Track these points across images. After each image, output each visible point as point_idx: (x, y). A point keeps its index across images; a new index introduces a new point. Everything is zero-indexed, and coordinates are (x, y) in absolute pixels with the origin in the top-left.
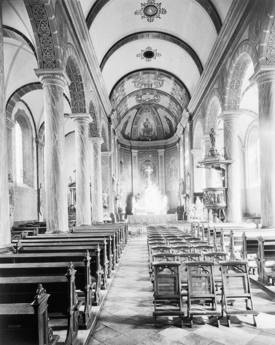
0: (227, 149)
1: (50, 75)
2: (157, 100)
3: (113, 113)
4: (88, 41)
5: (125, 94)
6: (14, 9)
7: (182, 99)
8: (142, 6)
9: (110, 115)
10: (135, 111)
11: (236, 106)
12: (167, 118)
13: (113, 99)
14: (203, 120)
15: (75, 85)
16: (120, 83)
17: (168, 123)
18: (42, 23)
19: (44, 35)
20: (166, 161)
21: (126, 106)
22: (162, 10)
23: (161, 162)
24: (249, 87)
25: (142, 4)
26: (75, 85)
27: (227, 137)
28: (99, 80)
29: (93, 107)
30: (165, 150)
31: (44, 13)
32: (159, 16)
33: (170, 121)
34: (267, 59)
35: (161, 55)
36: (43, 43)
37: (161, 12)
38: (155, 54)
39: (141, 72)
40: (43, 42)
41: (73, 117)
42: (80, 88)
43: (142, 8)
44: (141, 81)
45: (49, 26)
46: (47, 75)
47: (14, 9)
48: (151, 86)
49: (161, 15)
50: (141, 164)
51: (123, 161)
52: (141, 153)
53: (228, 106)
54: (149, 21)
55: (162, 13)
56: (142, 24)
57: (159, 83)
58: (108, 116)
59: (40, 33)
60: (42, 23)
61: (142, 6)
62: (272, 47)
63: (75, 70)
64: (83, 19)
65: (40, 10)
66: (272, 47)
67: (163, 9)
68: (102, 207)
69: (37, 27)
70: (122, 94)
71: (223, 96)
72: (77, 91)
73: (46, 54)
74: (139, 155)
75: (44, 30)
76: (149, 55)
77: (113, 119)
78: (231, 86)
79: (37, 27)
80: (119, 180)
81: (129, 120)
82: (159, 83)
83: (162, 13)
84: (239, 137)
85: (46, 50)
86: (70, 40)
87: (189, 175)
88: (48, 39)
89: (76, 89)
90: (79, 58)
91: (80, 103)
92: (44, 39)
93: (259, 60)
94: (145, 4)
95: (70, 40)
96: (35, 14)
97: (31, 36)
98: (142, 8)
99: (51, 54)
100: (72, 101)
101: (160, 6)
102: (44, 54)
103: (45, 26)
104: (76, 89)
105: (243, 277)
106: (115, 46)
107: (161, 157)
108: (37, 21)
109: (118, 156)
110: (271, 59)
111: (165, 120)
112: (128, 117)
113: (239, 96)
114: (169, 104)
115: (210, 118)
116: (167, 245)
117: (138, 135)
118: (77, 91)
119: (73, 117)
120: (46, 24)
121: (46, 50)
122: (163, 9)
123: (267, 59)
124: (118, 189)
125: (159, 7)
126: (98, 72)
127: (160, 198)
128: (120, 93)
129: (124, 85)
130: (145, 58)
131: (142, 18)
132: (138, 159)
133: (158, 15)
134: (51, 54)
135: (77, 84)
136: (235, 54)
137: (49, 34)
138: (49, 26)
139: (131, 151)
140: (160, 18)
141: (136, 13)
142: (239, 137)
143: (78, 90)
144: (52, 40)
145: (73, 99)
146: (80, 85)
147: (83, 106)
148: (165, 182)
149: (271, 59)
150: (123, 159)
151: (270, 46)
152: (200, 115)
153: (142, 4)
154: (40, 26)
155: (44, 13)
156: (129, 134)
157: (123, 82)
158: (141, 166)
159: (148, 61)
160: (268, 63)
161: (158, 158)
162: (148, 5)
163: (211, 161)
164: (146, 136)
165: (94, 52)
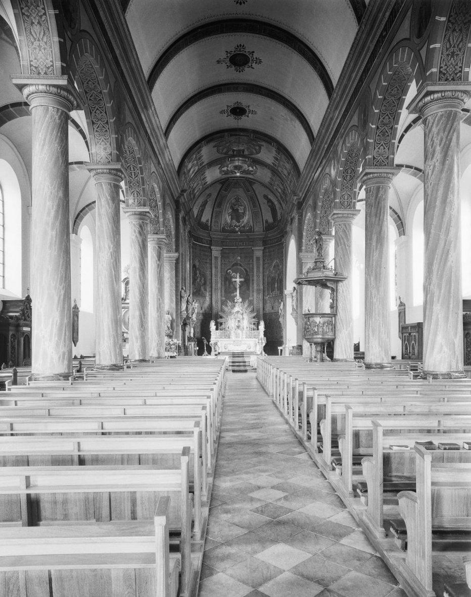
0: (337, 260)
1: (105, 171)
2: (252, 171)
3: (183, 195)
4: (151, 110)
5: (203, 163)
7: (289, 175)
8: (227, 54)
9: (179, 197)
10: (219, 186)
11: (351, 202)
12: (268, 198)
13: (184, 172)
14: (314, 213)
15: (132, 169)
16: (195, 148)
17: (269, 206)
18: (97, 109)
19: (99, 123)
20: (266, 265)
21: (203, 179)
22: (255, 59)
23: (258, 268)
24: (412, 123)
25: (227, 52)
26: (132, 169)
27: (338, 244)
28: (163, 153)
29: (154, 191)
30: (265, 248)
31: (101, 99)
32: (252, 65)
33: (273, 203)
34: (374, 158)
35: (260, 62)
36: (96, 131)
38: (248, 111)
39: (226, 134)
40: (98, 130)
41: (128, 212)
42: (138, 173)
43: (228, 57)
44: (227, 145)
45: (106, 113)
46: (101, 170)
48: (243, 153)
49: (254, 65)
50: (226, 269)
51: (197, 264)
52: (227, 251)
53: (341, 202)
55: (256, 63)
56: (228, 74)
57: (255, 150)
58: (176, 198)
59: (94, 120)
60: (97, 109)
61: (227, 54)
62: (380, 144)
63: (133, 151)
64: (144, 81)
65: (97, 96)
66: (380, 144)
67: (256, 58)
69: (91, 113)
70: (197, 163)
71: (365, 140)
72: (133, 177)
74: (224, 255)
75: (99, 117)
76: (238, 111)
77: (184, 204)
78: (343, 176)
79: (91, 113)
80: (191, 295)
81: (208, 200)
82: (255, 150)
84: (391, 208)
85: (95, 108)
86: (129, 119)
87: (295, 291)
88: (103, 127)
89: (133, 174)
90: (258, 408)
91: (138, 192)
92: (98, 127)
93: (366, 157)
94: (231, 52)
95: (129, 119)
96: (90, 100)
97: (82, 122)
98: (228, 57)
100: (126, 189)
101: (253, 55)
103: (101, 113)
104: (133, 174)
105: (318, 395)
107: (258, 259)
108: (92, 107)
109: (190, 257)
110: (379, 158)
111: (266, 201)
112: (207, 195)
113: (355, 190)
114: (271, 178)
115: (323, 212)
116: (123, 208)
117: (223, 222)
118: (133, 177)
119: (128, 212)
120: (103, 110)
122: (256, 58)
123: (374, 158)
124: (189, 308)
126: (162, 144)
127: (254, 324)
128: (195, 162)
129: (201, 150)
131: (228, 68)
132: (221, 261)
133: (250, 65)
135: (134, 168)
136: (349, 134)
137: (106, 121)
138: (106, 113)
139: (210, 248)
140: (253, 68)
141: (218, 62)
142: (391, 208)
143: (135, 175)
144: (109, 128)
145: (128, 187)
146: (138, 170)
147: (141, 196)
148: (263, 299)
149: (379, 158)
150: (197, 260)
151: (377, 143)
152: (311, 204)
153: (227, 52)
154: (95, 112)
155: (101, 99)
156: (207, 221)
157: (200, 147)
158: (227, 272)
159: (240, 72)
160: (375, 163)
161: (253, 261)
162: (235, 53)
163: (315, 277)
164: (235, 226)
165: (158, 122)
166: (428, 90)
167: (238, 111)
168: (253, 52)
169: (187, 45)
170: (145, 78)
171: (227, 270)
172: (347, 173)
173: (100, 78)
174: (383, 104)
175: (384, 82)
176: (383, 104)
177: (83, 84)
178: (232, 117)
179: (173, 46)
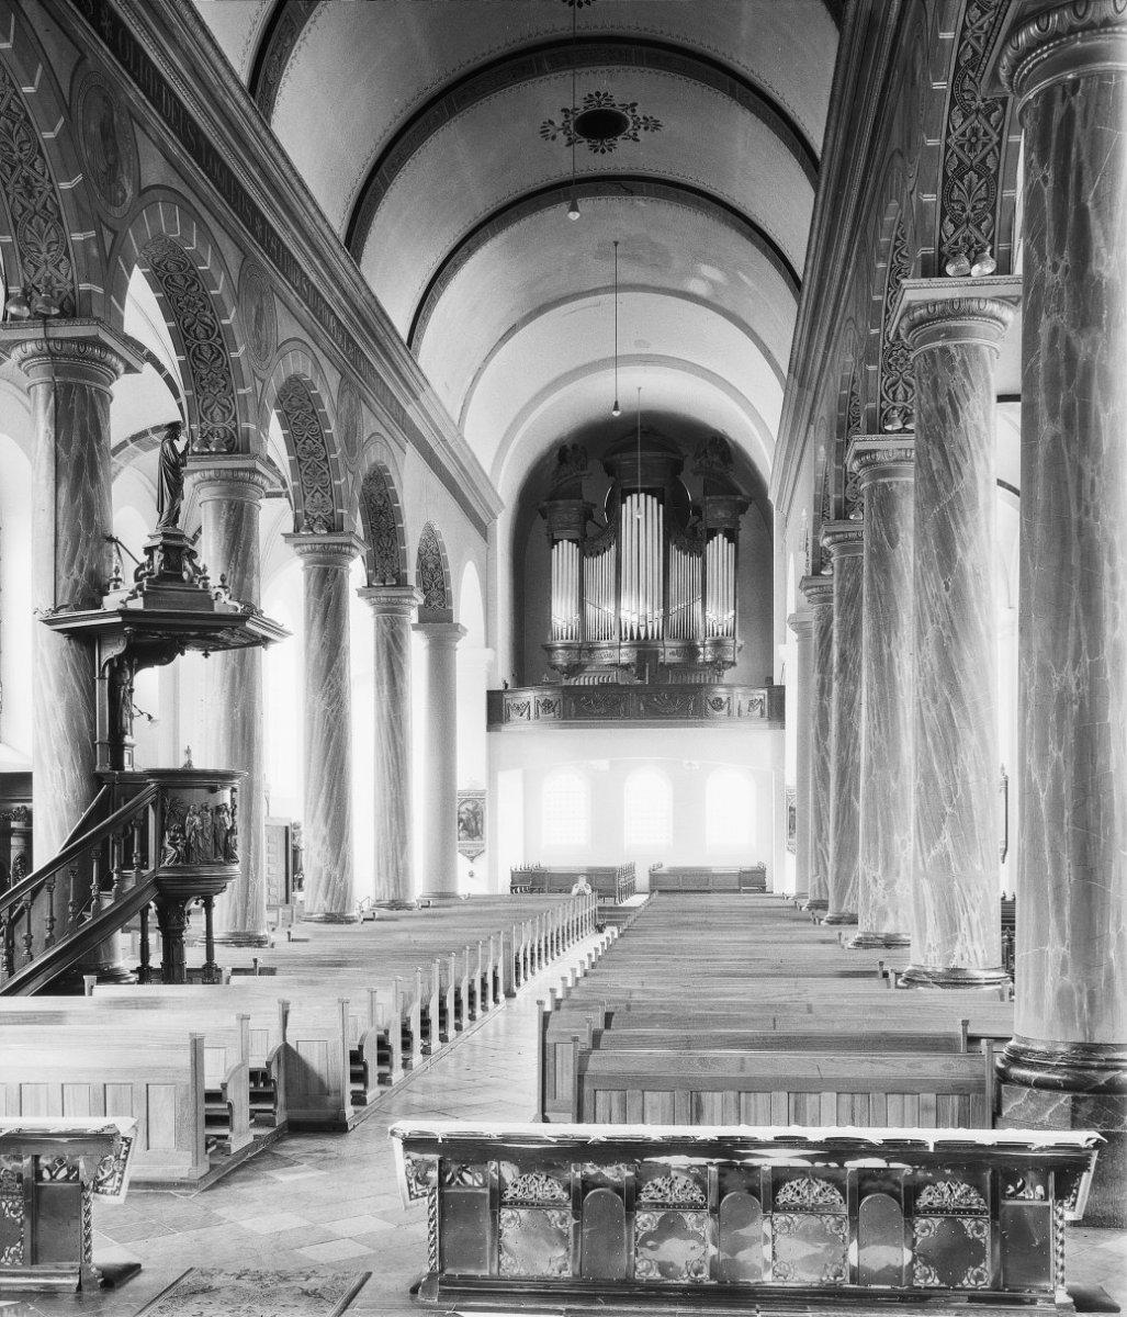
6: (599, 649)
22: (642, 120)
25: (564, 110)
32: (635, 134)
37: (642, 126)
46: (841, 536)
47: (599, 649)
54: (605, 95)
55: (646, 129)
67: (644, 118)
68: (580, 1125)
73: (313, 496)
83: (646, 129)
85: (302, 436)
99: (323, 496)
102: (309, 497)
106: (367, 197)
110: (310, 460)
121: (302, 436)
125: (631, 114)
130: (618, 109)
134: (323, 496)
137: (323, 457)
140: (638, 140)
149: (310, 460)
153: (564, 110)
166: (858, 448)
167: (600, 125)
168: (636, 104)
169: (452, 113)
170: (237, 81)
171: (903, 988)
172: (894, 400)
173: (27, 90)
174: (851, 402)
175: (485, 1195)
176: (851, 402)
177: (282, 402)
178: (584, 145)
179: (411, 125)
